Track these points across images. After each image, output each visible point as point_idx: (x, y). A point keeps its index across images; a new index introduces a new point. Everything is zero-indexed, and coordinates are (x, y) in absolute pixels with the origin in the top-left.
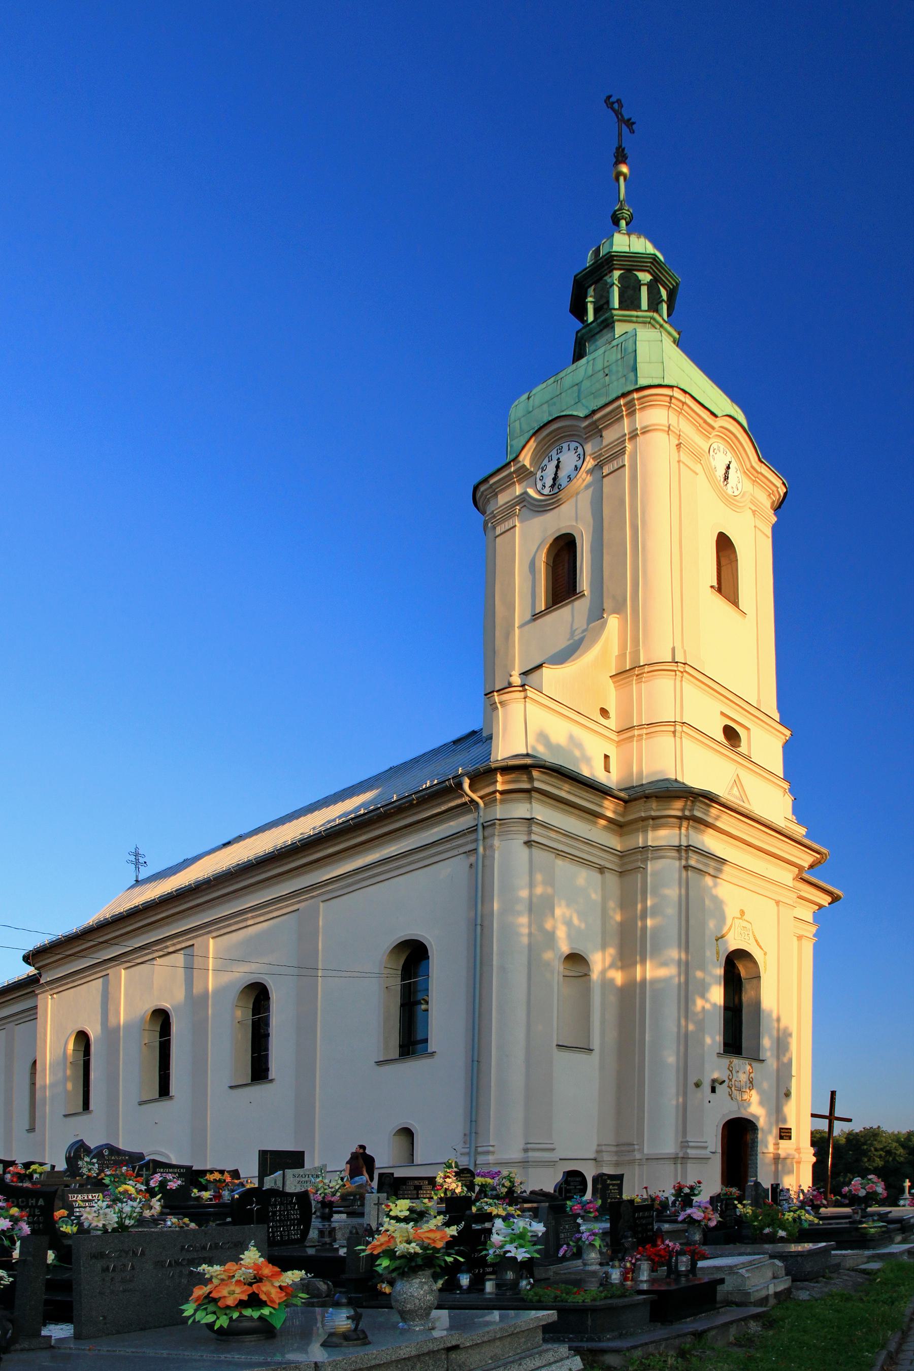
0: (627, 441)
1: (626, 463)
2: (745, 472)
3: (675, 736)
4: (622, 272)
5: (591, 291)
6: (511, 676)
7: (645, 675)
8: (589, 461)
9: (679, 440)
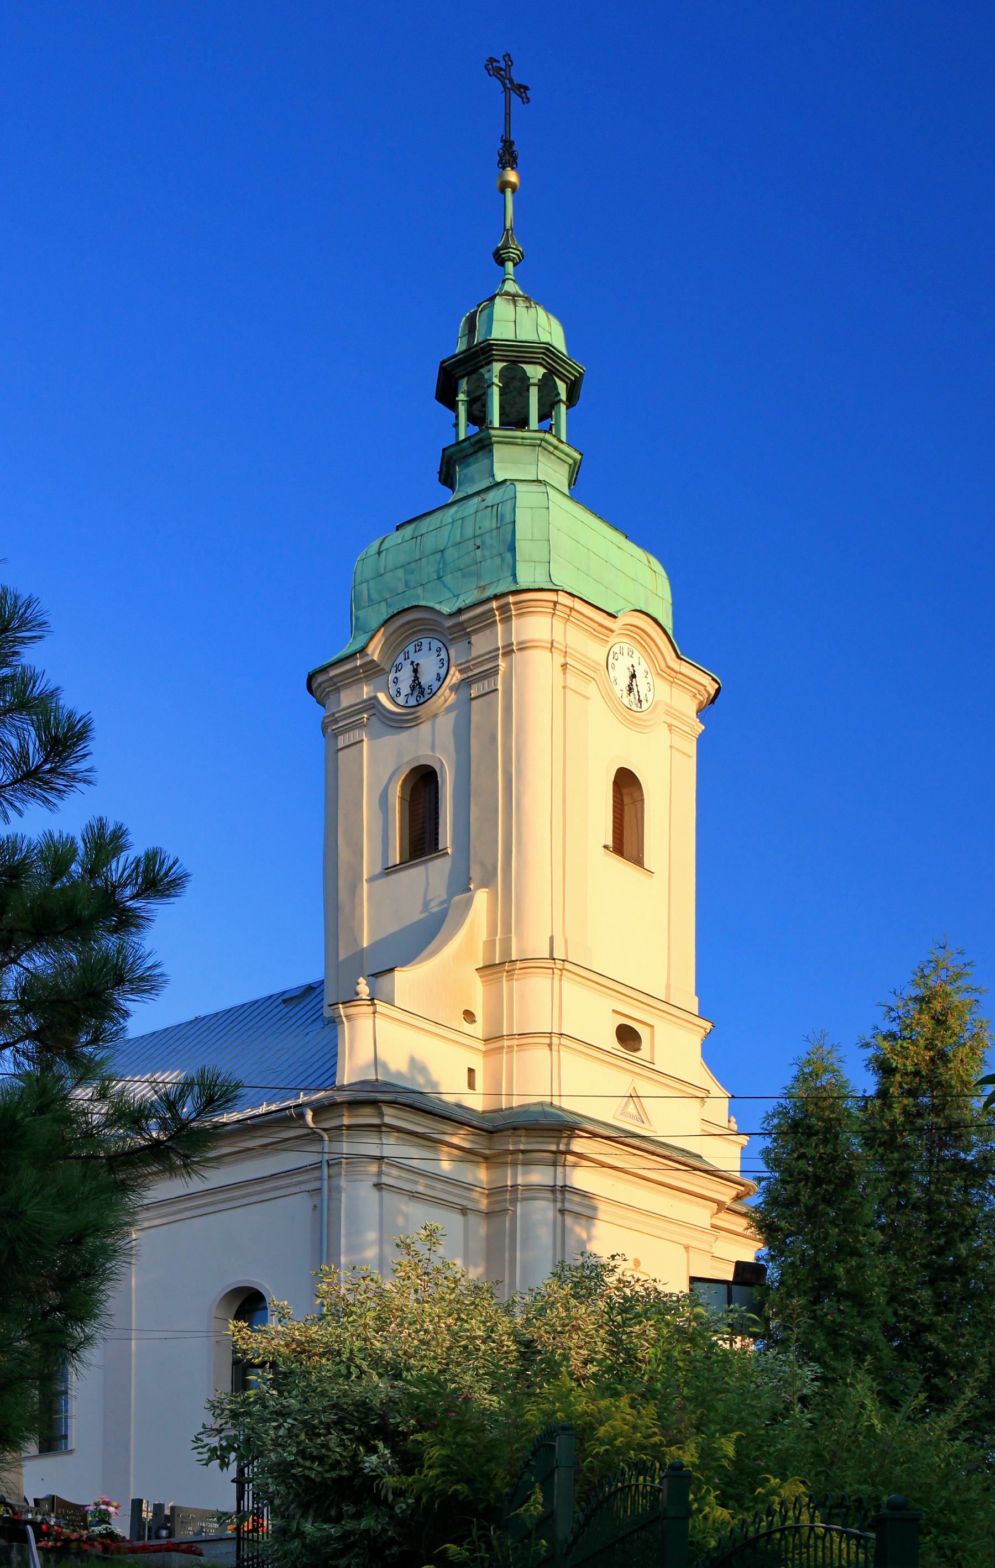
0: (500, 656)
1: (500, 687)
3: (551, 1049)
4: (505, 364)
5: (463, 385)
6: (358, 984)
7: (516, 972)
8: (454, 674)
9: (565, 657)
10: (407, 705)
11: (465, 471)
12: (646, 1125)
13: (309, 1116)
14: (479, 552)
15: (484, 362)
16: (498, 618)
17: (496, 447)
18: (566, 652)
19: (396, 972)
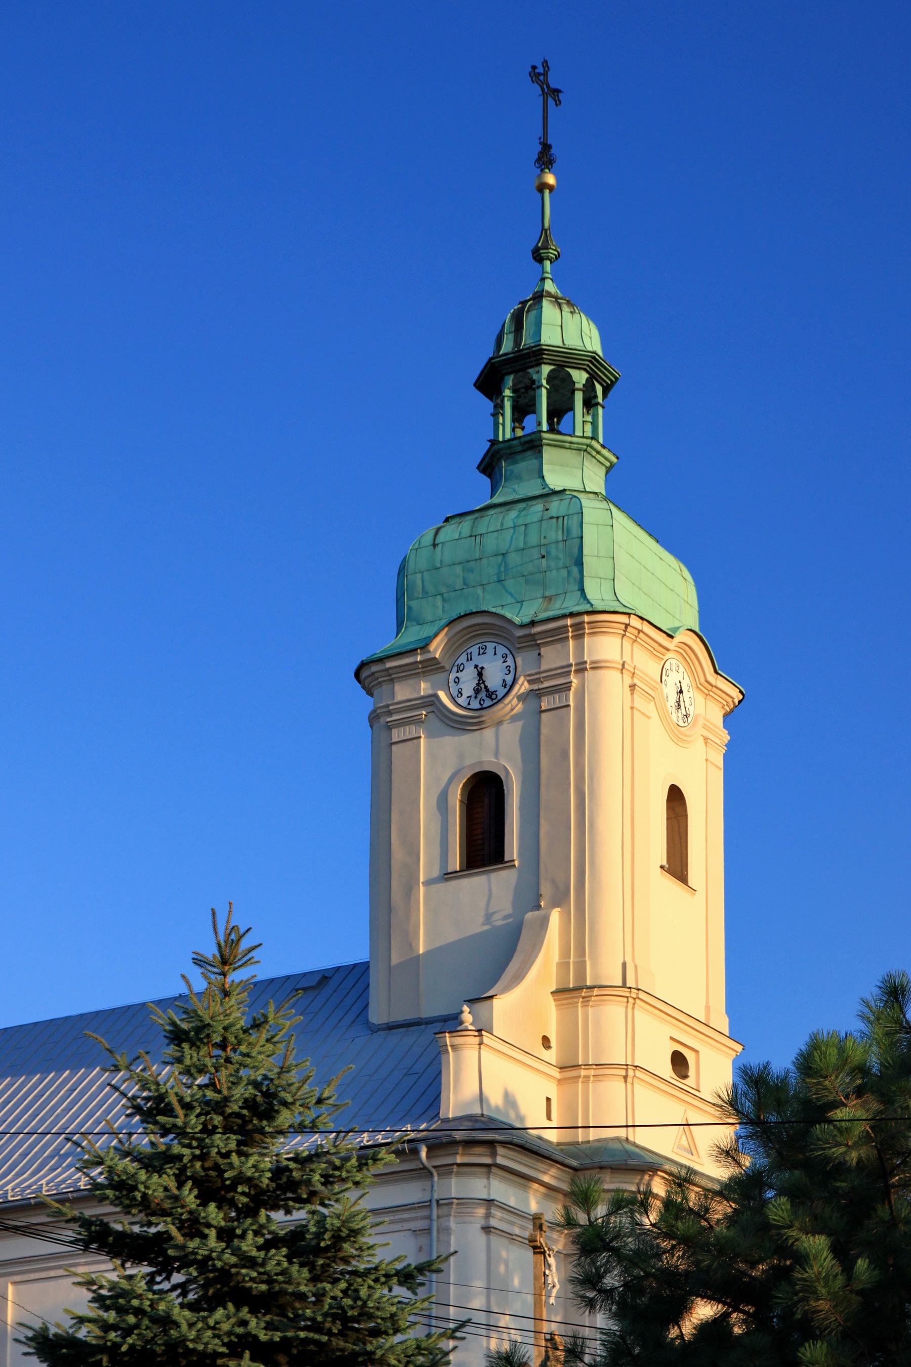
0: (572, 673)
1: (572, 703)
2: (698, 687)
3: (626, 1082)
4: (553, 367)
5: (510, 381)
7: (593, 998)
8: (522, 684)
9: (632, 677)
10: (469, 707)
11: (511, 467)
12: (694, 1158)
13: (423, 1154)
14: (543, 560)
15: (533, 363)
16: (570, 634)
17: (545, 448)
18: (634, 673)
19: (494, 1000)
